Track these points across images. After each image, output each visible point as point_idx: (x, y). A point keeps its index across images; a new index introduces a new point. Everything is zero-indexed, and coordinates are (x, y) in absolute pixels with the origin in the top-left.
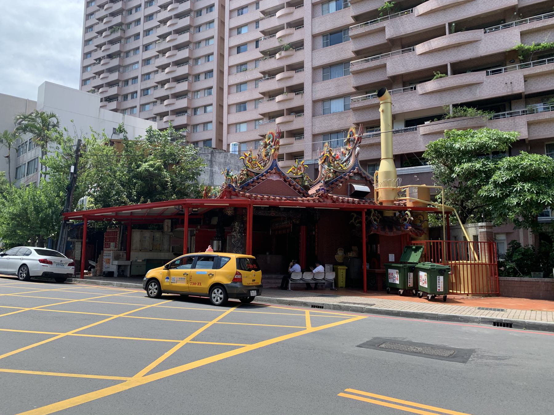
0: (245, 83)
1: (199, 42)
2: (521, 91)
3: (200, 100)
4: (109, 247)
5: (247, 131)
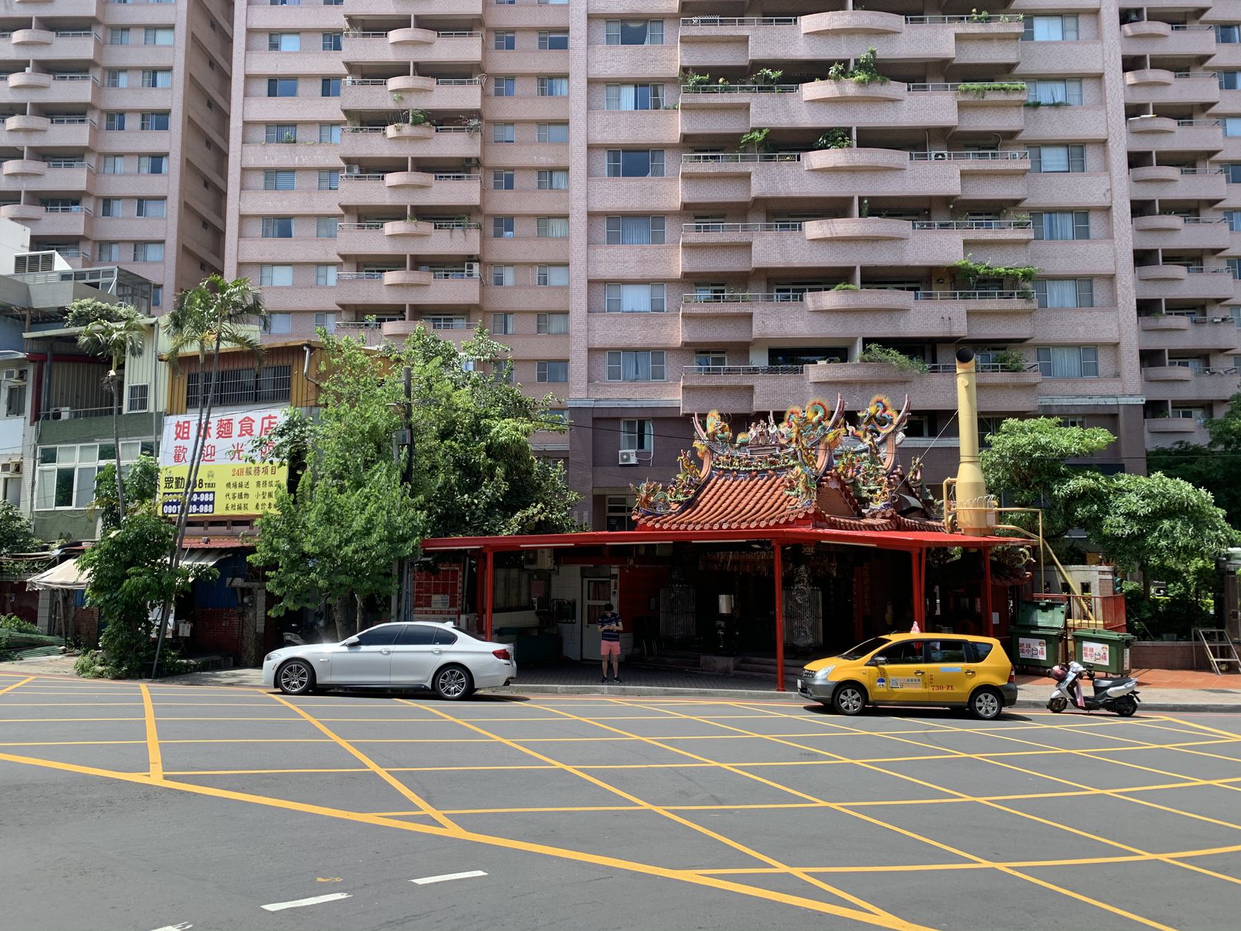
0: (292, 171)
1: (125, 29)
3: (127, 180)
4: (429, 605)
5: (294, 287)
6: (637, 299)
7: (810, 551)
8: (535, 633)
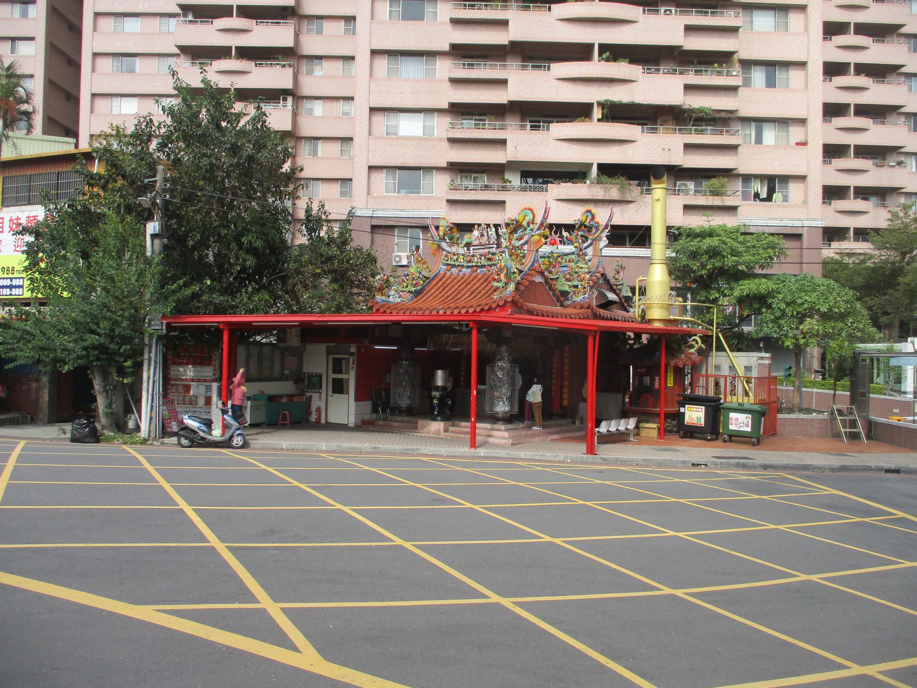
7: (508, 334)
8: (285, 400)
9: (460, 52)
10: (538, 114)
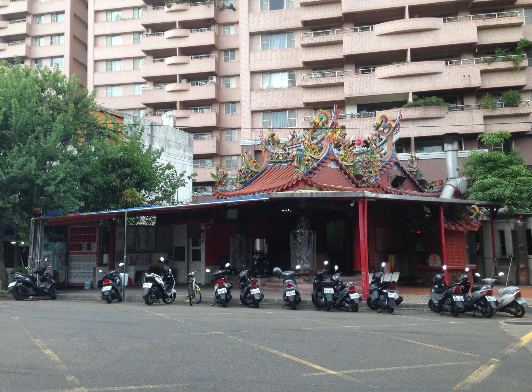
2: (477, 86)
3: (43, 49)
6: (281, 81)
9: (311, 26)
10: (365, 62)
